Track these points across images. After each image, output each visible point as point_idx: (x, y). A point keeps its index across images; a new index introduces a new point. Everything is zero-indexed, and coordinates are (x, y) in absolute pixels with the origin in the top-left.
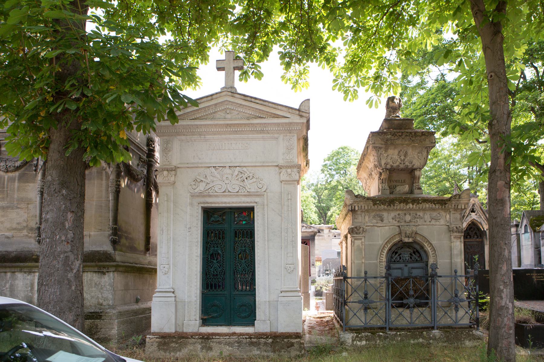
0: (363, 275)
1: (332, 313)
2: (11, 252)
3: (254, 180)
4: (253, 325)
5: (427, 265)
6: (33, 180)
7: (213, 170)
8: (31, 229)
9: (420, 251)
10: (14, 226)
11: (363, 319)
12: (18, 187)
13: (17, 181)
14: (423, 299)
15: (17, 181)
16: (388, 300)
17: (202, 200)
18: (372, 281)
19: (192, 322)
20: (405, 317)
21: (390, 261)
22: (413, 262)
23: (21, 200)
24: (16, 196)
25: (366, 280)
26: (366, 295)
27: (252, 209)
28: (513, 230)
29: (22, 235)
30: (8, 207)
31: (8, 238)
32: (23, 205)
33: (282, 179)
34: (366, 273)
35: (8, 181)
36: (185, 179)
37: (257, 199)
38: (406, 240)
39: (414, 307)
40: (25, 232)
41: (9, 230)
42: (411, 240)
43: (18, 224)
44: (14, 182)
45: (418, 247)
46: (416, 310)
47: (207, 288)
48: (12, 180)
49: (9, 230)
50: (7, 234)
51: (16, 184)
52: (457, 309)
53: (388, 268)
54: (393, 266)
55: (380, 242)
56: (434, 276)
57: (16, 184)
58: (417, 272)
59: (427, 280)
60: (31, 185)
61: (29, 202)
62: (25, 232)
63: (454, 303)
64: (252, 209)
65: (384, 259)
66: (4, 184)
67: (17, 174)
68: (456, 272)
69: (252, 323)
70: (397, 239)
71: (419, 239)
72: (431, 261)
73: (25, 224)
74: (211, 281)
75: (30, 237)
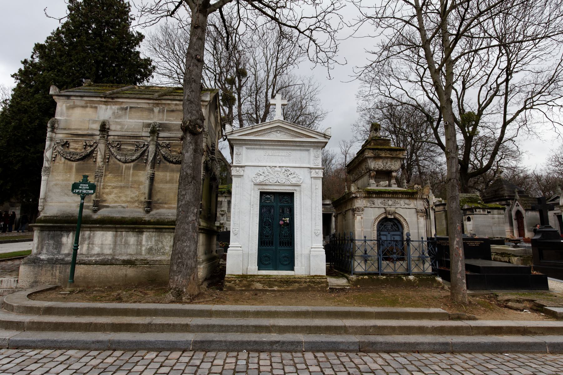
0: (363, 238)
1: (71, 234)
2: (125, 218)
3: (294, 175)
4: (293, 269)
5: (402, 233)
6: (144, 169)
7: (268, 168)
8: (141, 202)
9: (398, 224)
10: (129, 199)
11: (364, 267)
12: (133, 173)
13: (132, 169)
14: (403, 256)
15: (132, 169)
16: (380, 255)
17: (261, 187)
18: (368, 242)
19: (253, 268)
20: (388, 267)
21: (379, 230)
22: (393, 231)
23: (134, 182)
24: (131, 179)
25: (365, 242)
26: (366, 251)
27: (293, 193)
28: (426, 67)
29: (134, 206)
30: (124, 187)
31: (123, 207)
32: (136, 186)
33: (312, 176)
34: (365, 237)
35: (125, 169)
36: (249, 174)
37: (296, 188)
38: (389, 217)
39: (397, 260)
40: (136, 204)
41: (125, 202)
42: (392, 217)
43: (131, 198)
44: (130, 169)
45: (396, 222)
46: (397, 263)
47: (261, 245)
48: (129, 168)
49: (125, 202)
50: (123, 205)
51: (131, 171)
52: (424, 263)
53: (379, 235)
54: (382, 233)
55: (373, 218)
56: (408, 240)
57: (131, 171)
58: (398, 238)
59: (403, 244)
60: (142, 172)
61: (140, 183)
62: (136, 204)
63: (422, 259)
64: (293, 193)
65: (376, 229)
66: (122, 171)
67: (132, 164)
68: (422, 238)
69: (293, 269)
70: (384, 216)
71: (397, 216)
72: (405, 231)
73: (136, 199)
74: (264, 241)
75: (140, 208)
